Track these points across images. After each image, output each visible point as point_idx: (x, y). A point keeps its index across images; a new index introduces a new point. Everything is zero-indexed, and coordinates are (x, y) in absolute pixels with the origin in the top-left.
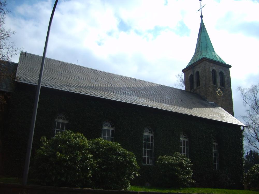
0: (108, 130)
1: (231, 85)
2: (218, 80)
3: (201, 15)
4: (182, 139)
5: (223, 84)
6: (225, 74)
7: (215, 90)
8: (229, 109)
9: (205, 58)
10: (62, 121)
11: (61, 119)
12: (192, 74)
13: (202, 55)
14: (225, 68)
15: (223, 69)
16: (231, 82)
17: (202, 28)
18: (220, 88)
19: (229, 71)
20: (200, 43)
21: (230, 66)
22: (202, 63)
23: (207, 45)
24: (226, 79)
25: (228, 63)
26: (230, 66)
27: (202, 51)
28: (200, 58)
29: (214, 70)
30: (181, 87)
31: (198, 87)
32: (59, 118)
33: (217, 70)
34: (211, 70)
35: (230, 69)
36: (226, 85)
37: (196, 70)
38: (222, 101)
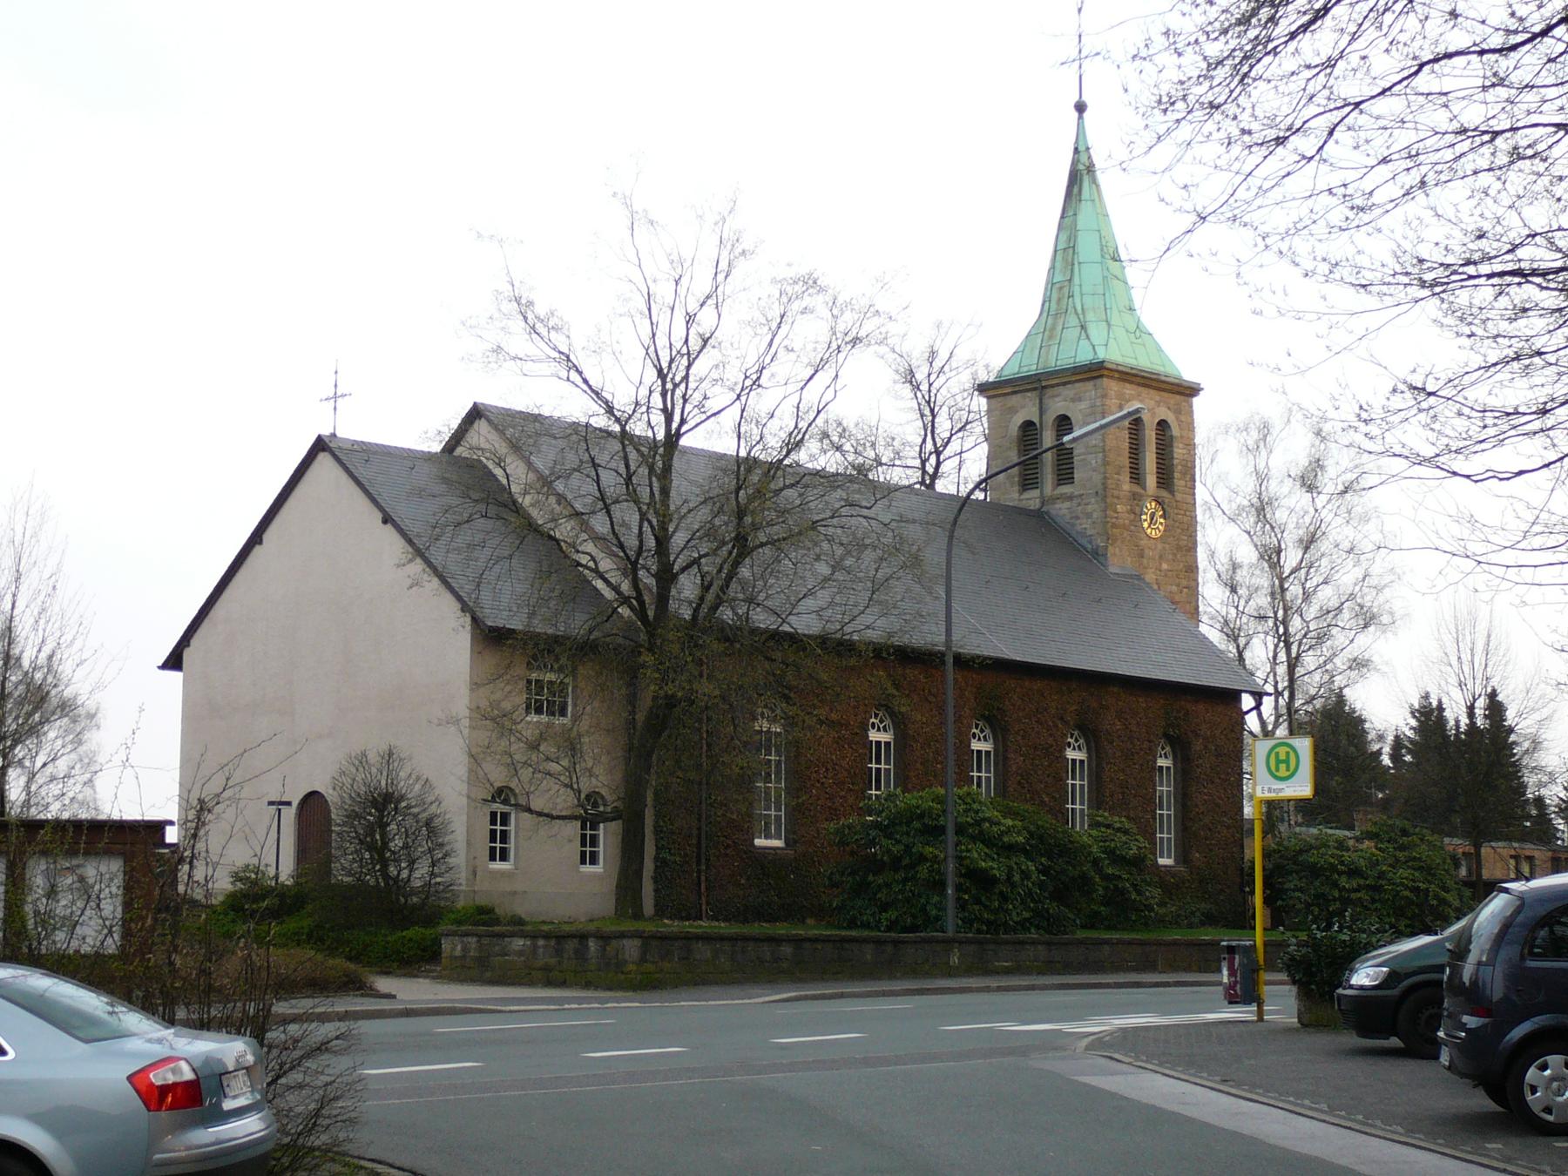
4: (1071, 754)
5: (1165, 480)
6: (1175, 431)
7: (1137, 510)
10: (884, 737)
12: (1036, 420)
13: (1088, 337)
19: (1191, 413)
21: (1191, 391)
22: (1090, 385)
25: (1189, 375)
26: (1191, 391)
31: (1066, 489)
35: (1195, 400)
36: (1179, 483)
37: (1058, 404)
38: (1161, 557)
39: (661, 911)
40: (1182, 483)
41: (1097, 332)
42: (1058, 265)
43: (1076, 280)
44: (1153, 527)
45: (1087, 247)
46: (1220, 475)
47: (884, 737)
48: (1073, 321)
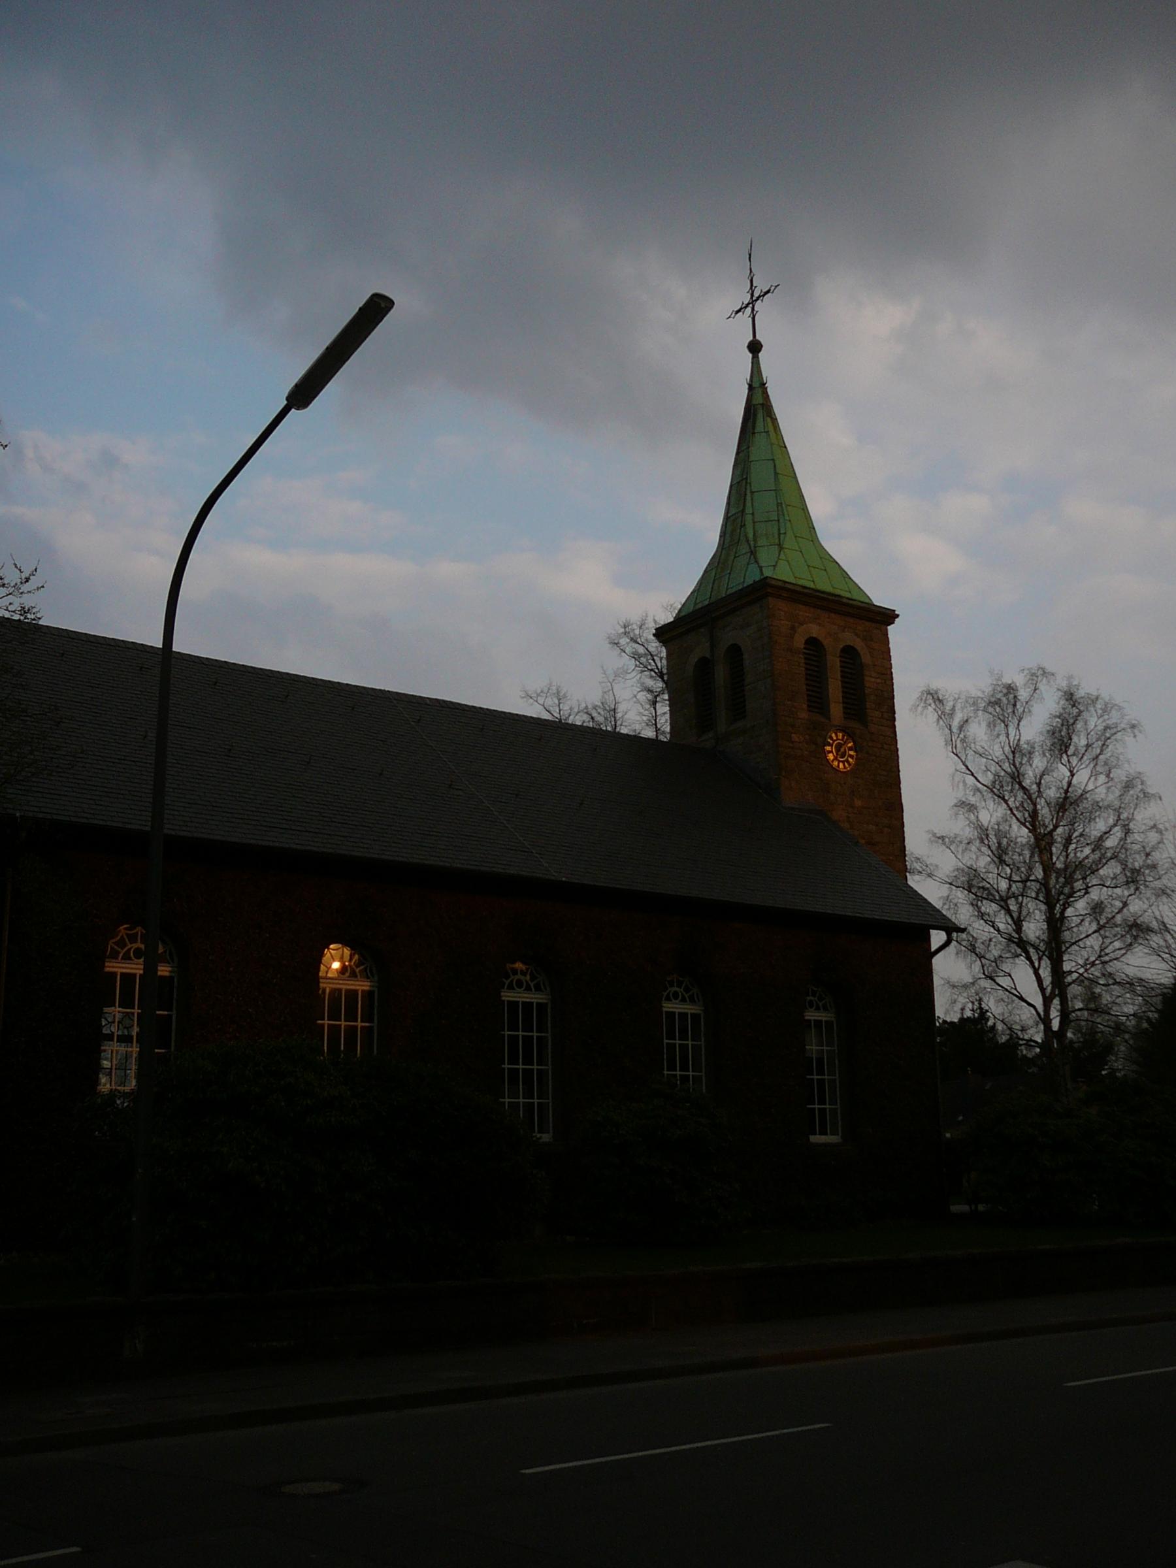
0: (122, 974)
1: (894, 713)
2: (835, 689)
3: (751, 338)
6: (866, 658)
8: (886, 830)
9: (773, 582)
10: (823, 1016)
11: (136, 961)
12: (708, 656)
13: (757, 562)
14: (868, 624)
15: (856, 635)
16: (893, 697)
17: (758, 411)
18: (841, 731)
20: (748, 498)
21: (889, 617)
23: (779, 505)
24: (871, 681)
25: (880, 599)
26: (889, 617)
27: (755, 540)
28: (749, 582)
29: (815, 639)
30: (638, 709)
32: (511, 987)
33: (826, 642)
34: (799, 642)
39: (170, 1010)
40: (877, 713)
41: (766, 556)
42: (732, 499)
43: (749, 510)
44: (838, 757)
45: (760, 476)
46: (917, 664)
47: (823, 1016)
48: (744, 548)
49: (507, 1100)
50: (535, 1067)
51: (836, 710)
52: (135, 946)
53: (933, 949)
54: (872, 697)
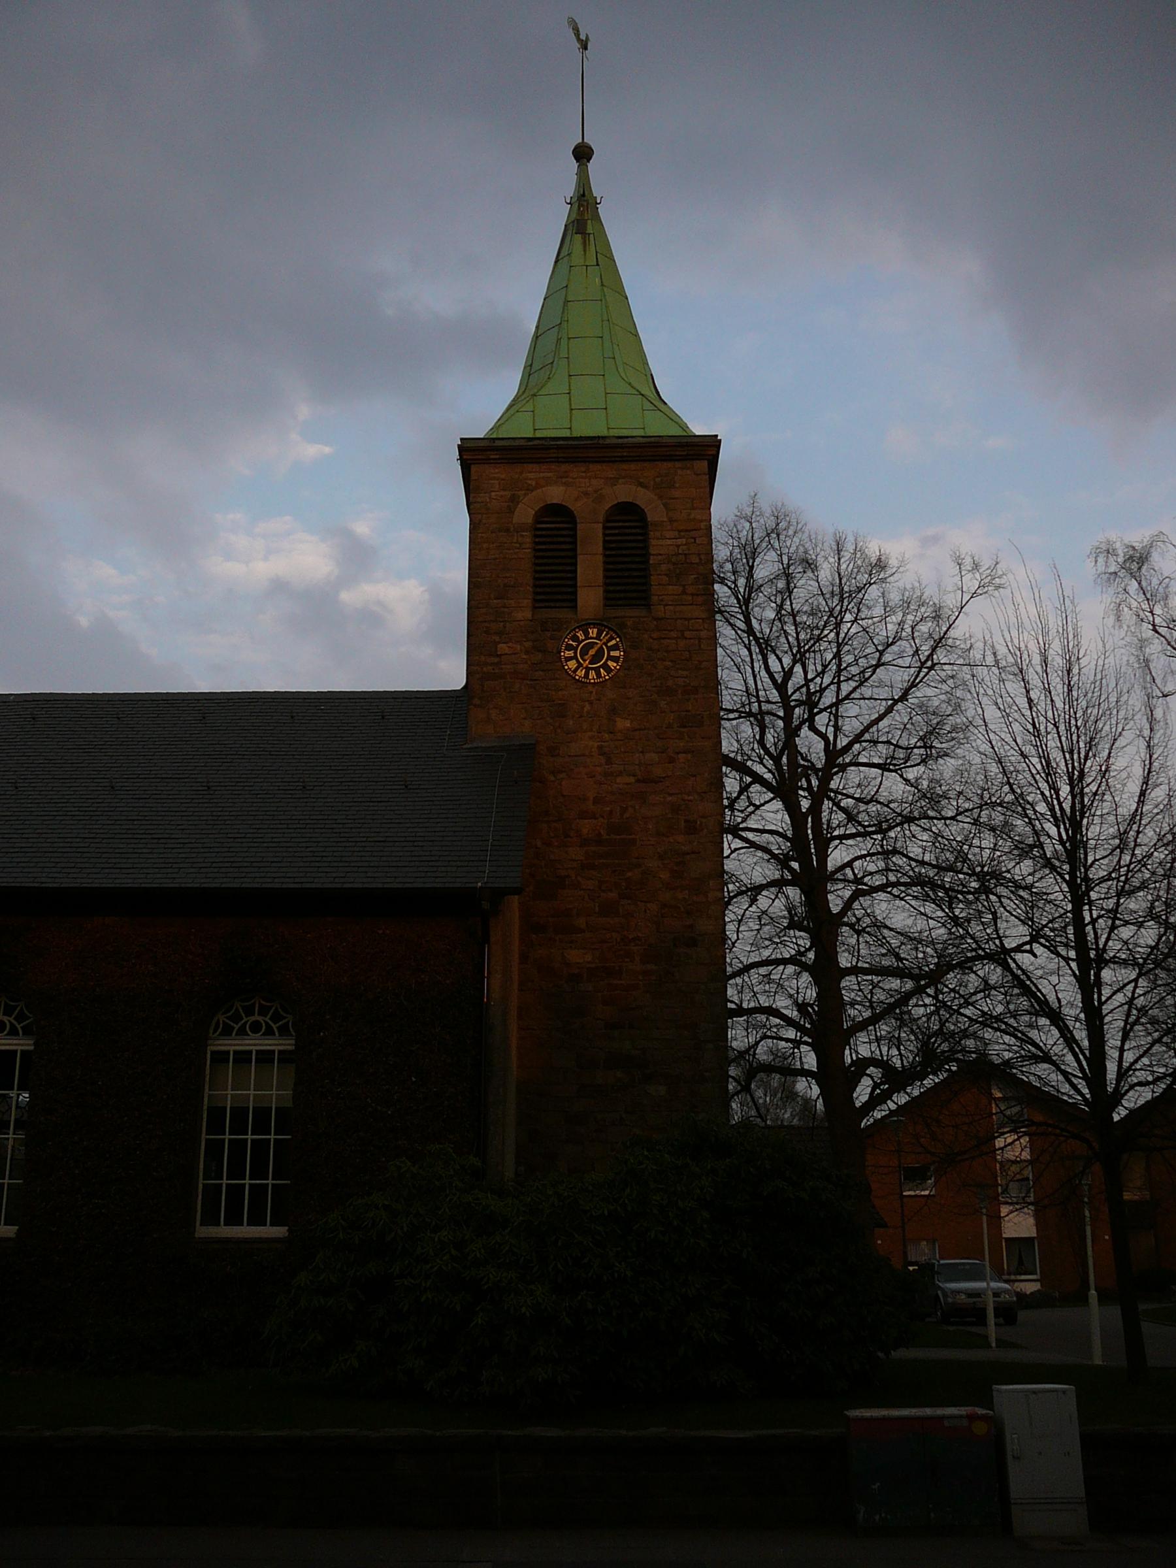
21: (705, 451)
33: (576, 507)
49: (270, 1182)
50: (272, 1137)
51: (590, 598)
52: (253, 1019)
53: (835, 910)
54: (664, 567)
